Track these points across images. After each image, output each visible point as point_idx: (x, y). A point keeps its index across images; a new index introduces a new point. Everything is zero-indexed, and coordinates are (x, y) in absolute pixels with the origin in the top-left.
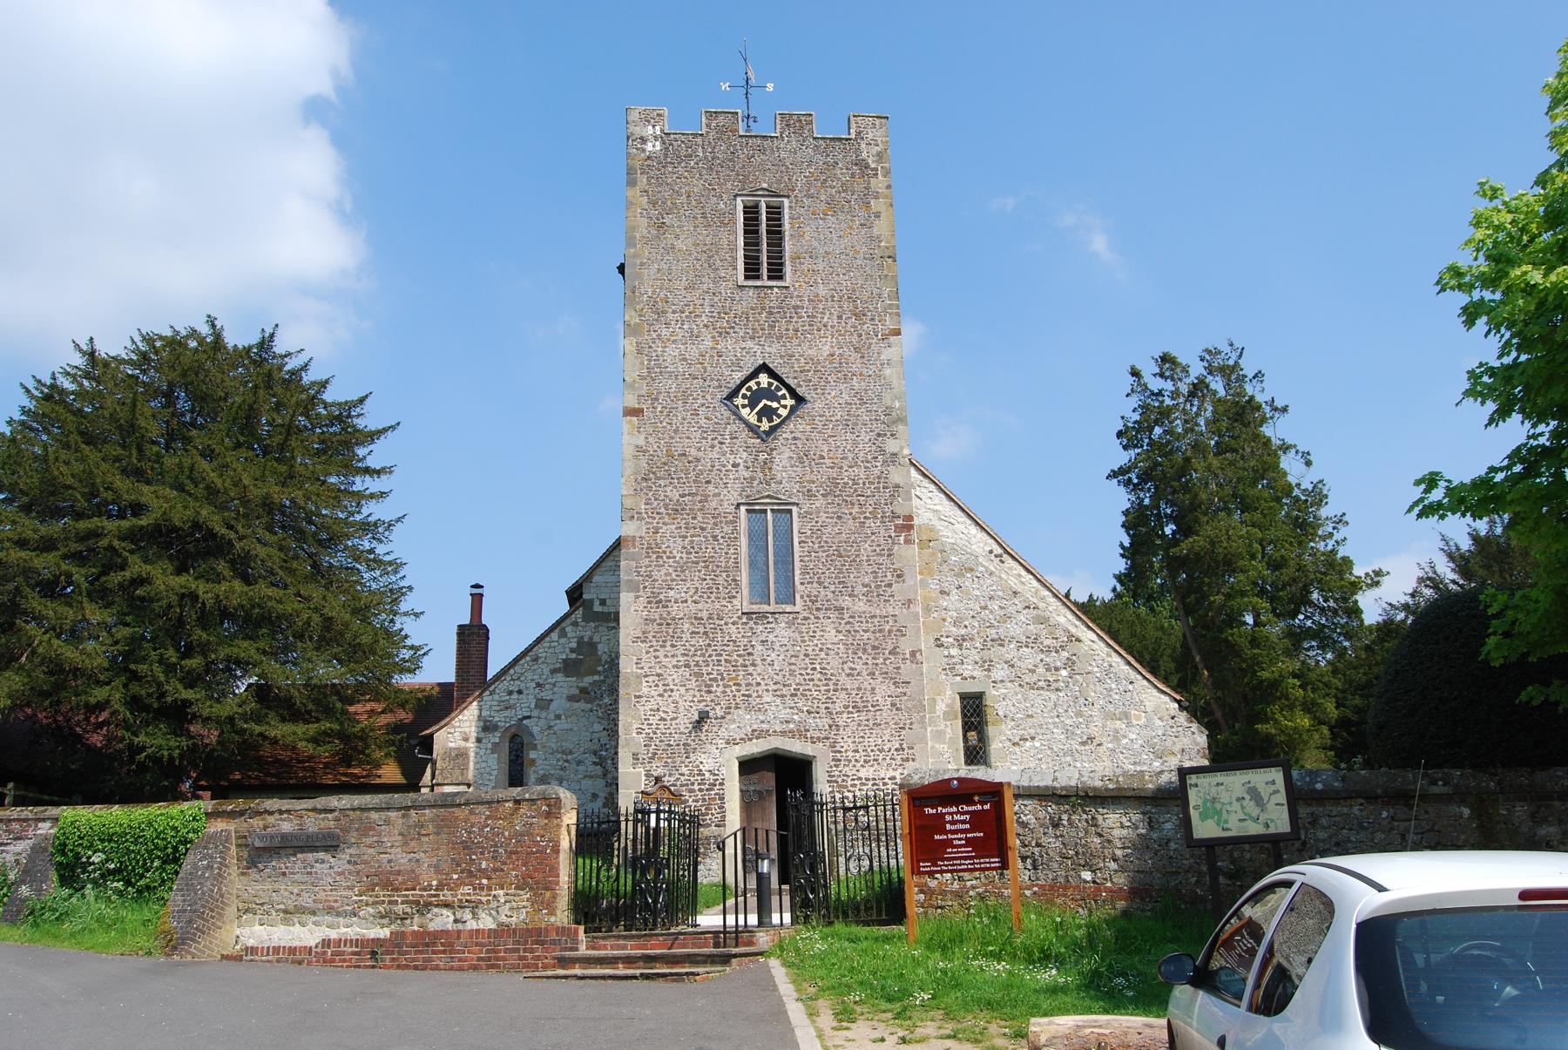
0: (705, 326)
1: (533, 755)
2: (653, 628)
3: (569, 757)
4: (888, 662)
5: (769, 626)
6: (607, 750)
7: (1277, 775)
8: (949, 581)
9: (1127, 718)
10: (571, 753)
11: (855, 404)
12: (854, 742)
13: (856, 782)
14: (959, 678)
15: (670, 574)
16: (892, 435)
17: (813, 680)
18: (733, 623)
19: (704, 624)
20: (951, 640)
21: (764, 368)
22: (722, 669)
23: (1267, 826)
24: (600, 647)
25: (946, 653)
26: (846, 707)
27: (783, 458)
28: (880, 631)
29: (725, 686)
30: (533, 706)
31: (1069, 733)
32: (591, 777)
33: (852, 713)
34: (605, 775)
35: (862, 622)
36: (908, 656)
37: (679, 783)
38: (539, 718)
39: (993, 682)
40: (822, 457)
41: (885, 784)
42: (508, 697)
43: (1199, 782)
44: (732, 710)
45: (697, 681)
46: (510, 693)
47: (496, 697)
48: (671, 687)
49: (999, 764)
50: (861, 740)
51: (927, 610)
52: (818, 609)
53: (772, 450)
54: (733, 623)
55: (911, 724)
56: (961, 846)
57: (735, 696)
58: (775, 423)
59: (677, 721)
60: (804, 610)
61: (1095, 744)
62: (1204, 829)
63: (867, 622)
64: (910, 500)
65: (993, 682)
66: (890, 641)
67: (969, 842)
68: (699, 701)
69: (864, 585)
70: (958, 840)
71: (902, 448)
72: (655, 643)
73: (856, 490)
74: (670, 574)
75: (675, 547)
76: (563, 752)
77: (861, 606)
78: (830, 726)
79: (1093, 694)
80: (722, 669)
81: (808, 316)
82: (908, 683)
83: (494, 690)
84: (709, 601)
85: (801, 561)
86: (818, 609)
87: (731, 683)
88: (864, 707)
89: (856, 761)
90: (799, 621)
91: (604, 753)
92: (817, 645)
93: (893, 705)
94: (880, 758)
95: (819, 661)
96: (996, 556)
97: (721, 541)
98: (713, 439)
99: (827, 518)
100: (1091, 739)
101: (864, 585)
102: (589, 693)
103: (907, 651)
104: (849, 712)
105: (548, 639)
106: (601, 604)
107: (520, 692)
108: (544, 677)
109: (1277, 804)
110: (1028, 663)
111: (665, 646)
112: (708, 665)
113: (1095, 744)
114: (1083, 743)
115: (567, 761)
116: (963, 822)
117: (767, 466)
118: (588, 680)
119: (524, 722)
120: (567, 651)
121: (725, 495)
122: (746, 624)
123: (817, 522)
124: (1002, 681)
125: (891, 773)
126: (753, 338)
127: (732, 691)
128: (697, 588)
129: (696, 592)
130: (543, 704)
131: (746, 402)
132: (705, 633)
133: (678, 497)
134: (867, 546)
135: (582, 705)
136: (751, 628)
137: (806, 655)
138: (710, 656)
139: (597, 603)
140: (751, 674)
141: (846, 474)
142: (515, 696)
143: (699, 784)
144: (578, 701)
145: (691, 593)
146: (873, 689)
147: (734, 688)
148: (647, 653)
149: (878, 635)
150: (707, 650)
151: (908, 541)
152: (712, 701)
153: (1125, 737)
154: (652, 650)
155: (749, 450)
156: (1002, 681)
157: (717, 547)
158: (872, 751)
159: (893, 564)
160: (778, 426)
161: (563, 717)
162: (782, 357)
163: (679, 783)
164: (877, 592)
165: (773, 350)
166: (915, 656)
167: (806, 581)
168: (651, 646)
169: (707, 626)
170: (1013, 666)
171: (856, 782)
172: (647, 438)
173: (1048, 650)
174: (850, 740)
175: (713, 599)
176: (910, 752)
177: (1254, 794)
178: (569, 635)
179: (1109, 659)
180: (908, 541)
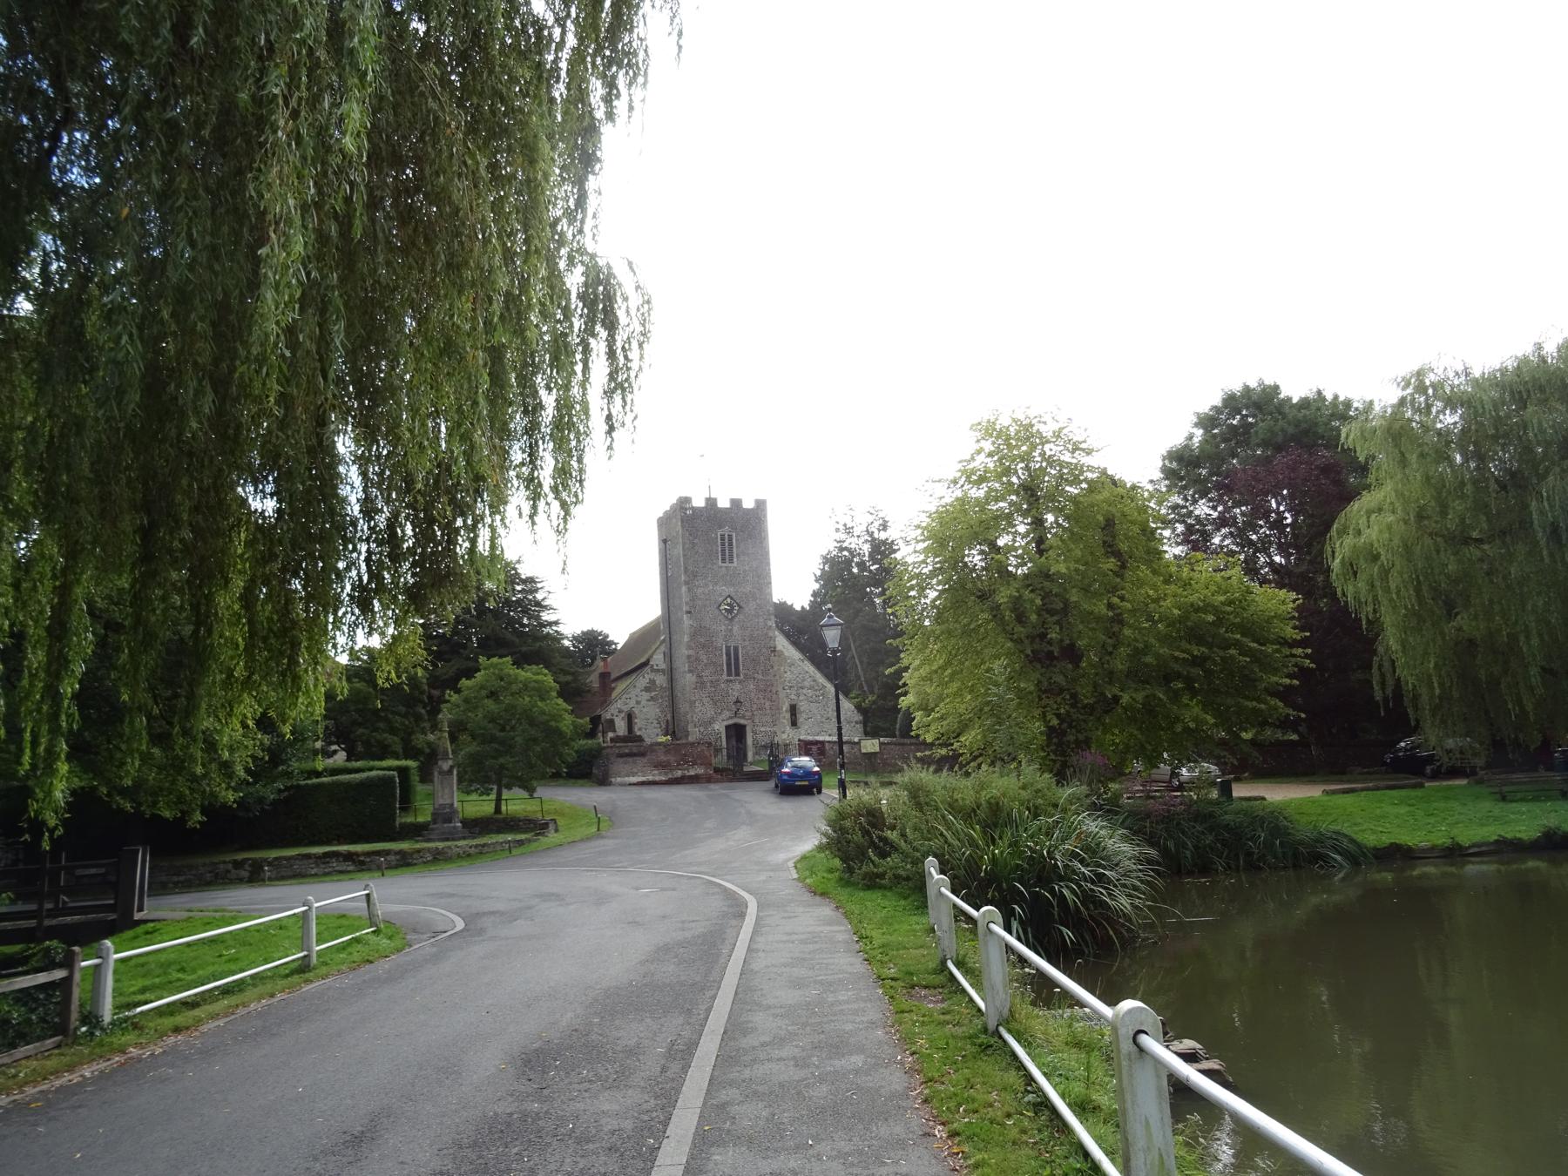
8: (787, 668)
62: (864, 751)
75: (704, 658)
109: (794, 723)
130: (638, 703)
164: (765, 673)
169: (714, 684)
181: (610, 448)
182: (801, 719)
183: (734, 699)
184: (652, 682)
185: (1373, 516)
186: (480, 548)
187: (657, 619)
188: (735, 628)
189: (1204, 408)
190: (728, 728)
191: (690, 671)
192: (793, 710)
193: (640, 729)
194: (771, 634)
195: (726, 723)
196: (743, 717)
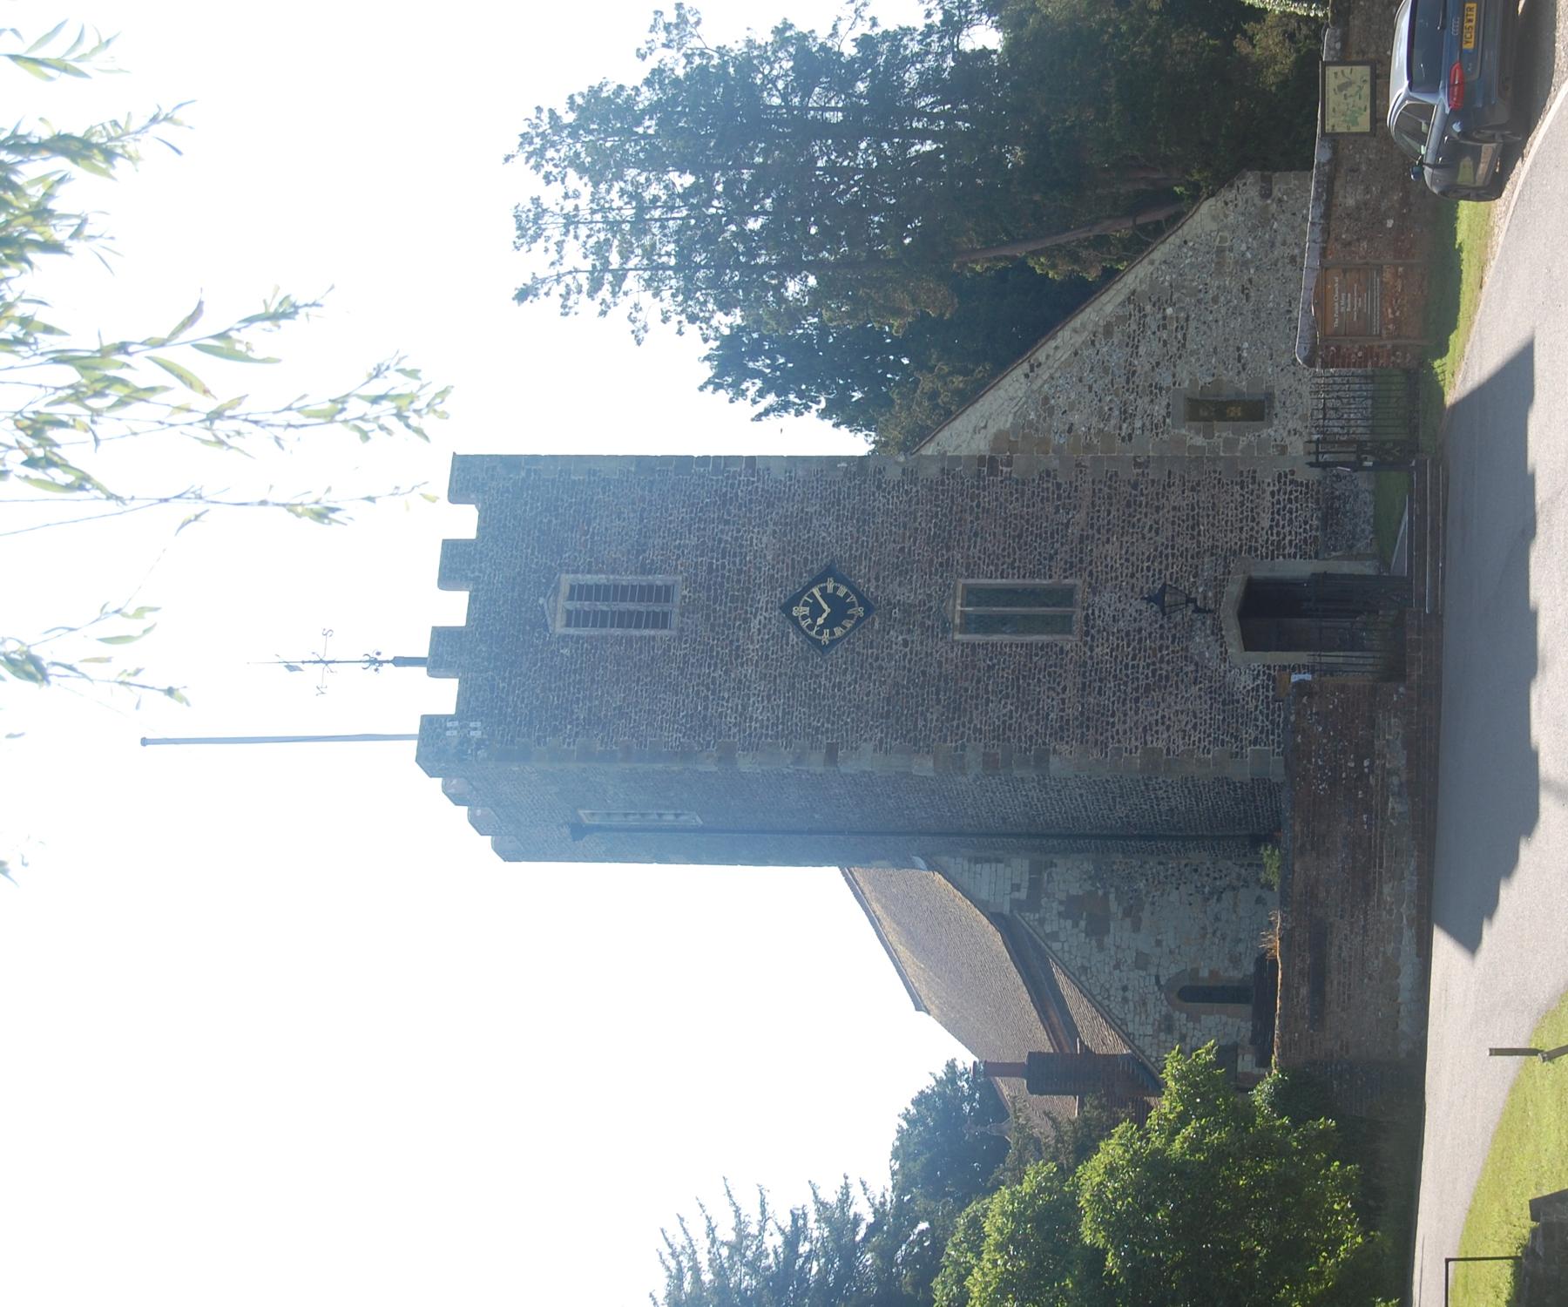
0: (726, 672)
1: (1205, 973)
3: (1210, 930)
4: (1145, 492)
5: (1097, 613)
6: (1204, 886)
7: (1331, 71)
8: (1058, 423)
9: (1223, 251)
10: (1204, 928)
11: (839, 510)
12: (1232, 532)
13: (1275, 532)
14: (1168, 420)
15: (1031, 716)
16: (880, 472)
17: (1160, 571)
18: (1091, 650)
19: (1090, 682)
20: (1125, 426)
21: (786, 608)
22: (1142, 663)
23: (1365, 81)
24: (1073, 892)
25: (1139, 432)
26: (1193, 537)
28: (1110, 498)
29: (1162, 661)
30: (1143, 973)
31: (1235, 312)
32: (1235, 904)
33: (1199, 531)
34: (1234, 889)
35: (1099, 517)
36: (1140, 471)
37: (1265, 711)
38: (1158, 965)
39: (1174, 384)
40: (902, 549)
41: (1278, 502)
42: (1131, 1004)
43: (1331, 124)
44: (1189, 655)
45: (1154, 690)
46: (1125, 1000)
47: (1130, 1017)
48: (1159, 717)
49: (1264, 386)
50: (1229, 524)
52: (1081, 561)
53: (889, 603)
54: (1091, 650)
55: (1215, 472)
56: (1362, 300)
57: (1173, 652)
58: (855, 599)
59: (1198, 712)
60: (1081, 575)
61: (1249, 286)
63: (1099, 511)
64: (960, 457)
65: (1174, 384)
66: (1122, 488)
68: (1177, 689)
69: (1057, 512)
71: (897, 463)
72: (1109, 734)
73: (944, 515)
74: (1031, 716)
76: (1204, 937)
77: (1081, 516)
78: (1212, 555)
79: (1195, 284)
80: (1142, 663)
81: (724, 558)
82: (1170, 472)
83: (1121, 1020)
84: (1064, 675)
85: (1024, 577)
86: (1081, 561)
87: (1159, 655)
88: (1193, 519)
89: (1252, 529)
90: (1093, 581)
91: (1207, 890)
92: (1122, 565)
93: (1193, 489)
94: (1249, 505)
95: (1139, 563)
96: (1032, 371)
97: (995, 661)
98: (872, 668)
99: (975, 547)
100: (1243, 289)
101: (1057, 512)
102: (1132, 906)
103: (1135, 471)
104: (1199, 534)
105: (1060, 954)
106: (1018, 890)
107: (1125, 989)
108: (1107, 959)
109: (1256, 410)
110: (1156, 346)
111: (1113, 723)
112: (1138, 679)
113: (1249, 286)
114: (1248, 297)
115: (1214, 933)
116: (1346, 298)
117: (907, 610)
118: (1114, 906)
119: (1162, 983)
120: (1076, 930)
121: (941, 656)
122: (1093, 637)
123: (980, 558)
124: (1174, 376)
126: (746, 621)
127: (1168, 654)
128: (1049, 689)
129: (1053, 689)
132: (1101, 680)
133: (940, 707)
134: (1011, 507)
135: (1145, 915)
136: (1099, 631)
137: (1132, 576)
138: (1127, 676)
139: (1016, 895)
140: (1150, 634)
141: (923, 525)
142: (1129, 995)
143: (1268, 691)
144: (1140, 919)
145: (1054, 695)
146: (1174, 508)
147: (1165, 652)
148: (1119, 742)
149: (1114, 501)
150: (1121, 679)
151: (1009, 463)
152: (1177, 675)
153: (1243, 255)
154: (1116, 737)
155: (887, 628)
156: (1174, 376)
157: (1002, 665)
158: (1242, 513)
159: (1034, 480)
160: (859, 595)
161: (1159, 937)
162: (773, 589)
163: (1265, 711)
165: (764, 598)
166: (1140, 463)
167: (1048, 573)
168: (1113, 738)
170: (1158, 364)
171: (1275, 532)
172: (865, 740)
173: (1143, 326)
174: (1229, 535)
175: (1062, 671)
176: (1245, 474)
177: (1342, 88)
178: (1055, 928)
179: (1157, 263)
180: (1009, 463)
181: (664, 1263)
183: (1150, 611)
185: (982, 425)
188: (903, 594)
190: (1251, 642)
191: (1042, 759)
193: (1235, 961)
194: (933, 471)
195: (1235, 650)
196: (1219, 585)
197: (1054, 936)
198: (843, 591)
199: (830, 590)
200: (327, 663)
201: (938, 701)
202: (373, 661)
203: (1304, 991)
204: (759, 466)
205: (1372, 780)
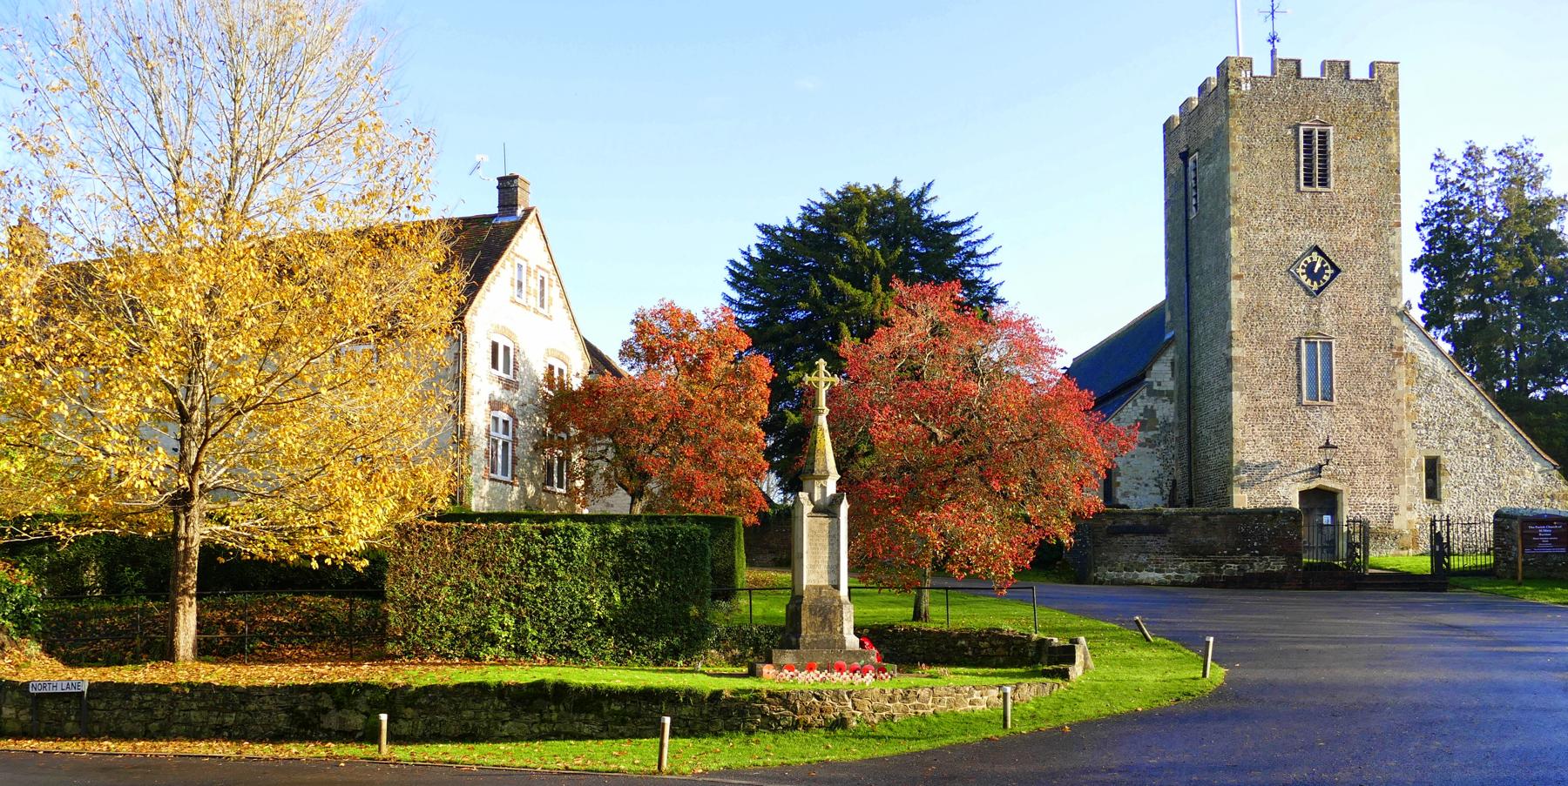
1: (1118, 479)
2: (1251, 412)
3: (1141, 482)
27: (1327, 306)
51: (1409, 406)
67: (1550, 541)
70: (1545, 540)
109: (1433, 493)
117: (1317, 313)
125: (1383, 501)
131: (1304, 271)
135: (1147, 449)
139: (1155, 384)
182: (1446, 484)
184: (1149, 412)
186: (1453, 578)
187: (1162, 304)
189: (678, 304)
192: (1433, 468)
193: (1125, 495)
197: (1135, 404)
198: (1325, 277)
199: (1326, 271)
200: (1273, 10)
201: (1267, 332)
202: (1274, 38)
203: (1128, 522)
204: (1396, 229)
205: (1247, 555)
